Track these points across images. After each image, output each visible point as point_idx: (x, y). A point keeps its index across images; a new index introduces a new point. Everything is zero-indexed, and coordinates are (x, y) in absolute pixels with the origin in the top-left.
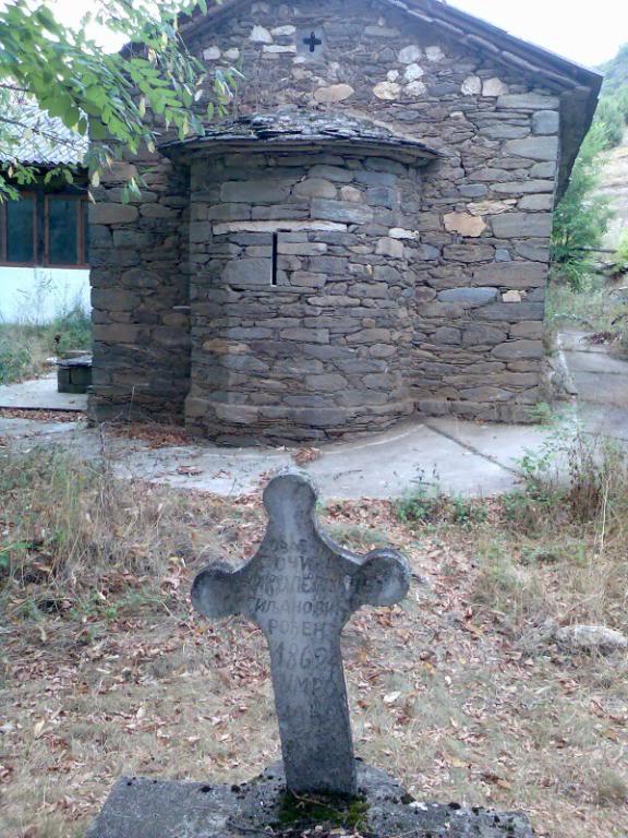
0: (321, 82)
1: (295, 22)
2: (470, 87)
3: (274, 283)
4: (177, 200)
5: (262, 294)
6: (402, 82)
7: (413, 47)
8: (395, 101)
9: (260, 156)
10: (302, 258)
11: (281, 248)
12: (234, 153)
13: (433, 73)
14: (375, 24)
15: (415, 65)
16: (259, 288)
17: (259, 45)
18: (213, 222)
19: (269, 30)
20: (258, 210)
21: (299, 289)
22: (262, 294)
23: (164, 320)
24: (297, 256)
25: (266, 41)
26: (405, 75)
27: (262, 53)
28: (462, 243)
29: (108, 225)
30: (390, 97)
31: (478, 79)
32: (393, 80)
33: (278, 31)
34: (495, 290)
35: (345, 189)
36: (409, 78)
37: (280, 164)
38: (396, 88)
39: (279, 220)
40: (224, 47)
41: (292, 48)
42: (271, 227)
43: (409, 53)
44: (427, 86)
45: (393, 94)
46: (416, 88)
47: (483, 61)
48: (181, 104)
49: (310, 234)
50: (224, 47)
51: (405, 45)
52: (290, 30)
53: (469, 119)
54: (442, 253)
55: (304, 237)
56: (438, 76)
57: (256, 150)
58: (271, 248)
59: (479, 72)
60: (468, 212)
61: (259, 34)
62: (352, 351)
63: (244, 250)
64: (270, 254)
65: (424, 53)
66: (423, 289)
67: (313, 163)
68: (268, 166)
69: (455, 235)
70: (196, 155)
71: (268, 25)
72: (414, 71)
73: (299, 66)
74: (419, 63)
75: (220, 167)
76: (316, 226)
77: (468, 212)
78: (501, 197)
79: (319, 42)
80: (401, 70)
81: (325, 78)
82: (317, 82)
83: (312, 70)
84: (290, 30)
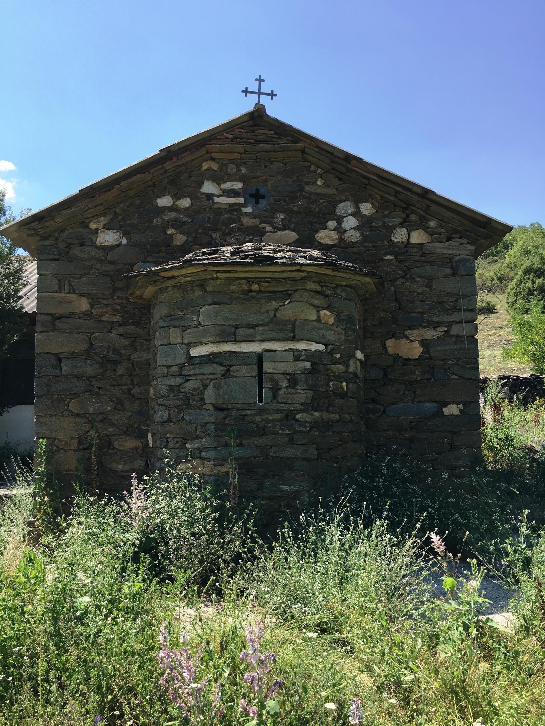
0: (268, 228)
1: (242, 179)
2: (400, 235)
3: (261, 401)
4: (132, 329)
5: (249, 412)
6: (339, 230)
7: (349, 203)
8: (334, 246)
9: (244, 281)
10: (288, 377)
11: (267, 367)
12: (217, 278)
13: (365, 223)
14: (315, 183)
15: (351, 217)
16: (245, 406)
17: (210, 196)
18: (191, 345)
19: (219, 184)
20: (241, 332)
21: (286, 407)
22: (249, 412)
23: (116, 444)
24: (283, 374)
25: (216, 193)
26: (343, 225)
27: (214, 203)
28: (404, 365)
29: (56, 354)
30: (330, 243)
31: (405, 230)
32: (333, 228)
33: (227, 186)
34: (435, 405)
35: (323, 312)
36: (346, 227)
37: (263, 289)
38: (335, 235)
39: (263, 341)
40: (177, 197)
41: (241, 200)
42: (256, 347)
43: (345, 208)
44: (362, 234)
45: (333, 240)
46: (353, 236)
47: (408, 216)
48: (305, 155)
49: (296, 354)
50: (177, 197)
51: (341, 201)
52: (238, 185)
53: (400, 261)
54: (385, 375)
55: (290, 357)
56: (371, 227)
57: (237, 275)
58: (256, 367)
59: (405, 224)
60: (408, 338)
61: (209, 187)
62: (335, 465)
63: (228, 370)
64: (255, 374)
65: (358, 207)
66: (371, 406)
67: (295, 288)
68: (251, 291)
69: (397, 357)
70: (170, 283)
71: (218, 179)
72: (350, 222)
73: (247, 214)
74: (353, 215)
75: (198, 293)
76: (301, 346)
77: (408, 338)
78: (435, 325)
79: (263, 197)
80: (340, 220)
81: (272, 225)
82: (265, 228)
83: (259, 218)
84: (238, 185)
